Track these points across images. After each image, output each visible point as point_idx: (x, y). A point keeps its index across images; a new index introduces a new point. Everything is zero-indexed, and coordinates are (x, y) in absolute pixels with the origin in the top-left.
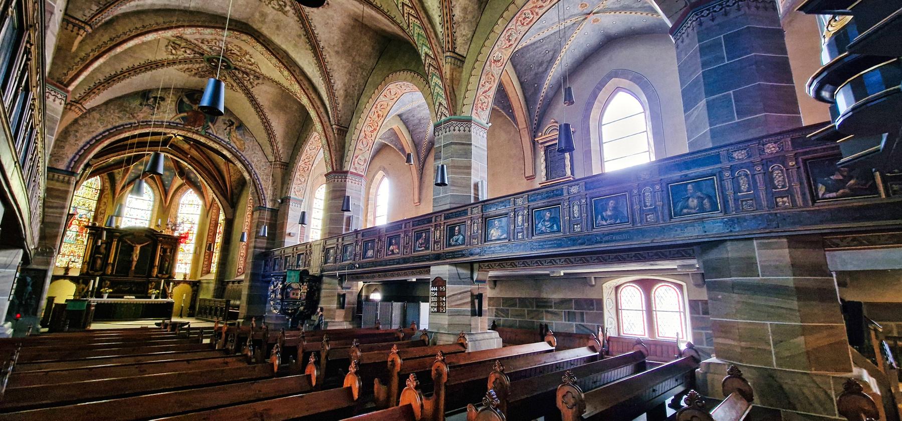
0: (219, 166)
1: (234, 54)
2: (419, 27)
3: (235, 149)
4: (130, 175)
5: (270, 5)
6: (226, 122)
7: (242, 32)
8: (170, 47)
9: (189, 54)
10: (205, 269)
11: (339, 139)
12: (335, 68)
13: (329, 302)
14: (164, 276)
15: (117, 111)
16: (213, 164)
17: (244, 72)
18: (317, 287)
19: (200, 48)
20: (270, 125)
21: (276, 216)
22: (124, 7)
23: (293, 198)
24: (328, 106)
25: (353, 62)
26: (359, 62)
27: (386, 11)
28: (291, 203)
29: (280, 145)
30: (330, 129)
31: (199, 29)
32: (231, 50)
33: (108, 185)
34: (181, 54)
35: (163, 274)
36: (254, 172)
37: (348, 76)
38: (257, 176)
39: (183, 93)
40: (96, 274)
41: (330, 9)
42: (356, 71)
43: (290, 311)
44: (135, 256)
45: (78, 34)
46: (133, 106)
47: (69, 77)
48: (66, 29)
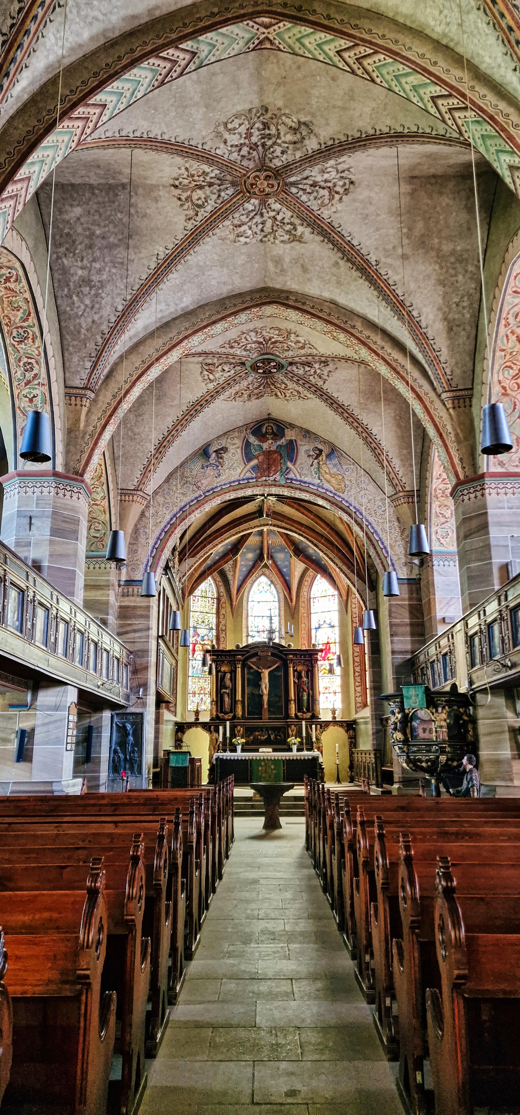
0: (334, 525)
1: (276, 342)
2: (478, 122)
3: (331, 492)
4: (240, 571)
5: (277, 241)
6: (312, 453)
7: (260, 305)
8: (205, 373)
9: (229, 371)
10: (359, 700)
11: (459, 416)
12: (412, 286)
13: (497, 745)
14: (305, 715)
15: (179, 486)
16: (328, 525)
17: (303, 364)
18: (469, 716)
19: (234, 356)
20: (370, 434)
21: (419, 590)
22: (117, 347)
23: (436, 552)
24: (423, 362)
25: (440, 258)
26: (453, 253)
27: (428, 130)
28: (435, 563)
29: (396, 463)
30: (438, 404)
31: (206, 330)
32: (270, 339)
33: (222, 589)
34: (220, 376)
35: (304, 713)
36: (367, 520)
37: (440, 290)
38: (373, 528)
39: (248, 431)
40: (226, 717)
41: (359, 190)
42: (453, 272)
43: (424, 765)
44: (263, 687)
45: (81, 405)
46: (194, 473)
47: (83, 462)
48: (70, 405)
